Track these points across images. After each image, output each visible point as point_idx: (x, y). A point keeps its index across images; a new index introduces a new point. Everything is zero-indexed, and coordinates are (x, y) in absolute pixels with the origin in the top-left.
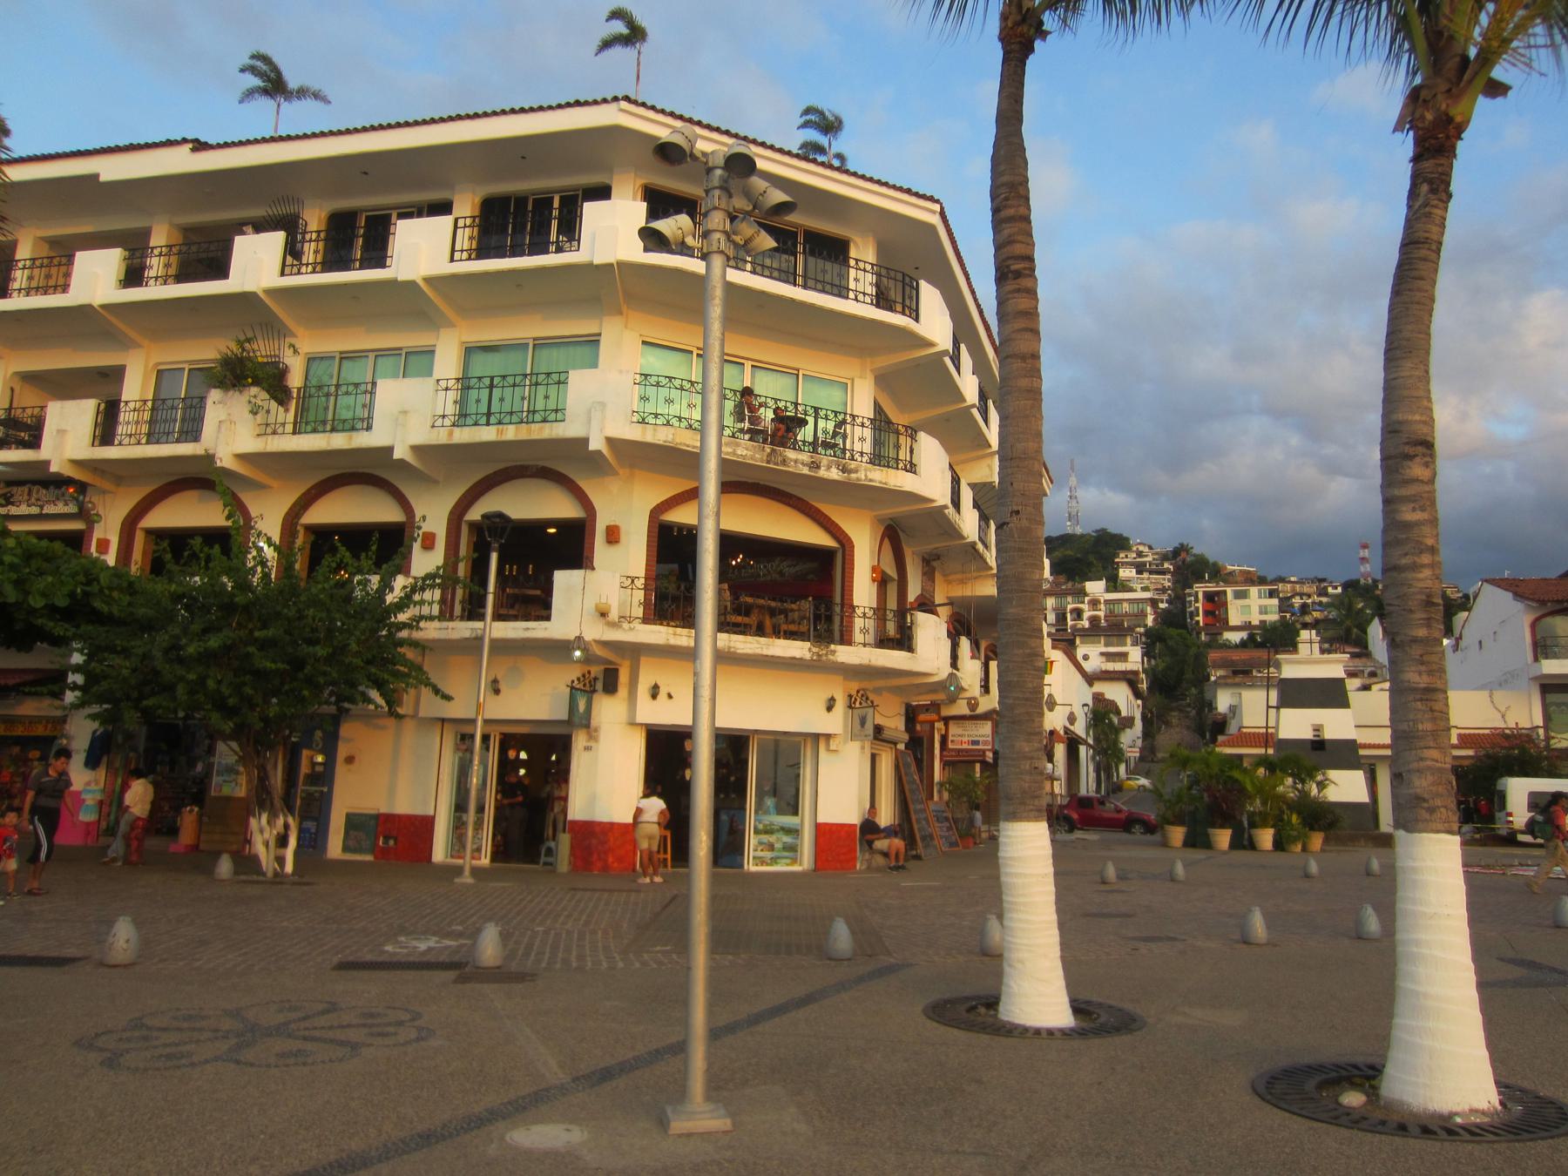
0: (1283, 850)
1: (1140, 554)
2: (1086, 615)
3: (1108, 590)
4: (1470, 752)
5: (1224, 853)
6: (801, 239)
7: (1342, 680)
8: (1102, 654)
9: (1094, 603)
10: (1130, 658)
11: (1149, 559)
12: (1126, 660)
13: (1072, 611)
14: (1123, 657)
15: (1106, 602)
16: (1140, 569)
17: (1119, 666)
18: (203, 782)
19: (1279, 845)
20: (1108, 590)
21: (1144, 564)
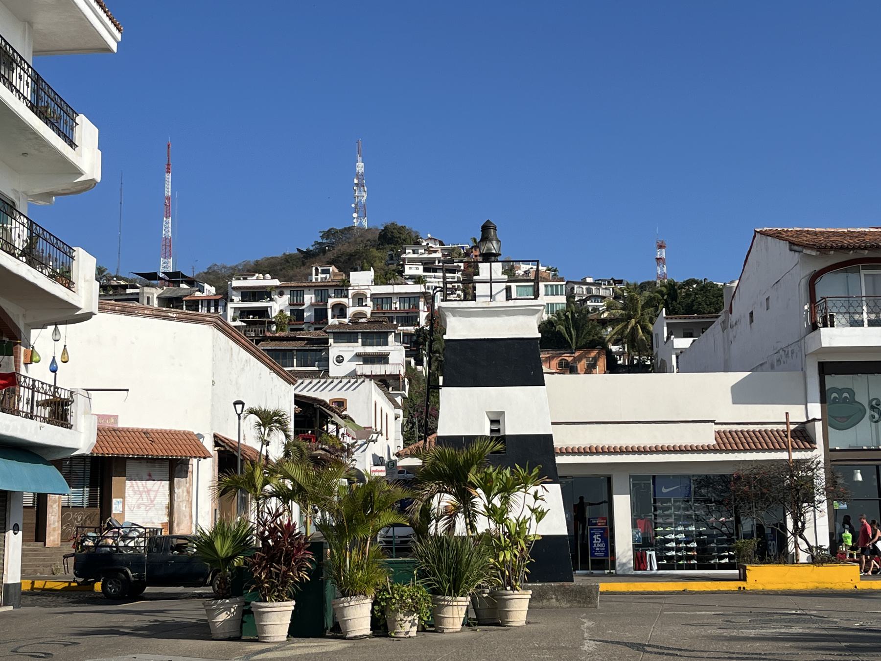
0: (386, 634)
1: (429, 250)
2: (350, 311)
3: (376, 282)
4: (416, 462)
5: (280, 646)
6: (866, 322)
7: (101, 309)
8: (358, 356)
9: (360, 299)
10: (391, 359)
11: (439, 255)
12: (387, 362)
13: (334, 307)
14: (383, 359)
15: (374, 297)
16: (429, 266)
17: (378, 369)
18: (278, 496)
19: (381, 625)
20: (376, 282)
21: (432, 261)
